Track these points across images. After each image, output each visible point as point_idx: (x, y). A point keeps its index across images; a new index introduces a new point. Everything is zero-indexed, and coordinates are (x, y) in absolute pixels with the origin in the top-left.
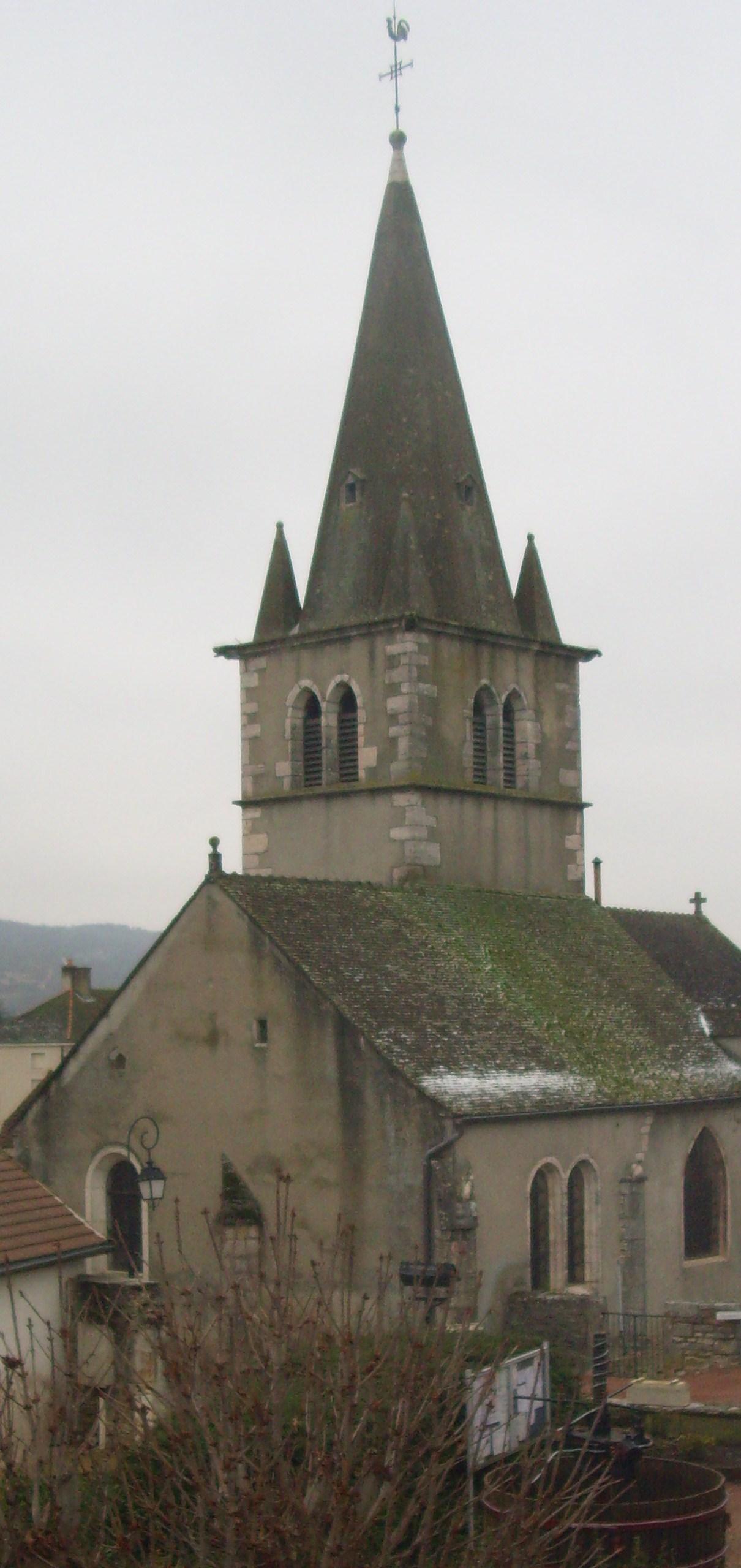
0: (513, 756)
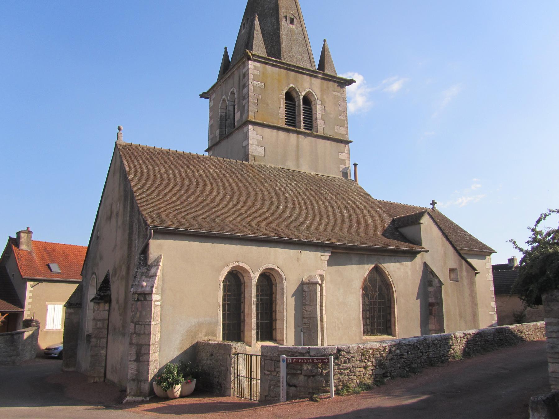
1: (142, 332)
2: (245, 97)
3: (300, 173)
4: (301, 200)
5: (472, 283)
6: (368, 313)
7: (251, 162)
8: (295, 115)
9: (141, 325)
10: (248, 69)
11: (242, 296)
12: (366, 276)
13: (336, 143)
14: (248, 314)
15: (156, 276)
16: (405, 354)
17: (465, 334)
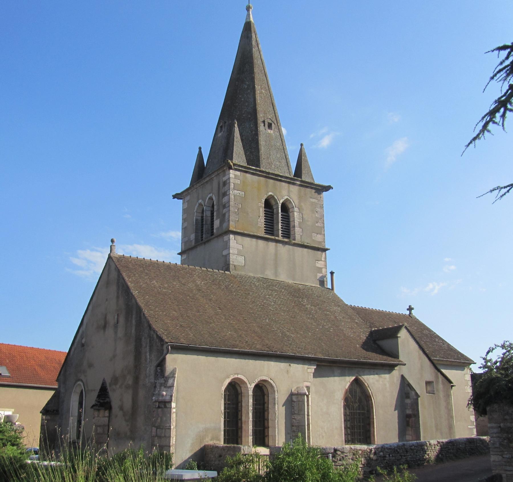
0: (289, 227)
1: (163, 435)
2: (226, 206)
3: (279, 283)
4: (284, 313)
5: (448, 396)
6: (349, 423)
7: (233, 272)
8: (273, 223)
9: (162, 429)
10: (229, 178)
11: (240, 405)
12: (347, 387)
13: (313, 251)
14: (245, 422)
15: (173, 386)
16: (387, 456)
17: (439, 442)
